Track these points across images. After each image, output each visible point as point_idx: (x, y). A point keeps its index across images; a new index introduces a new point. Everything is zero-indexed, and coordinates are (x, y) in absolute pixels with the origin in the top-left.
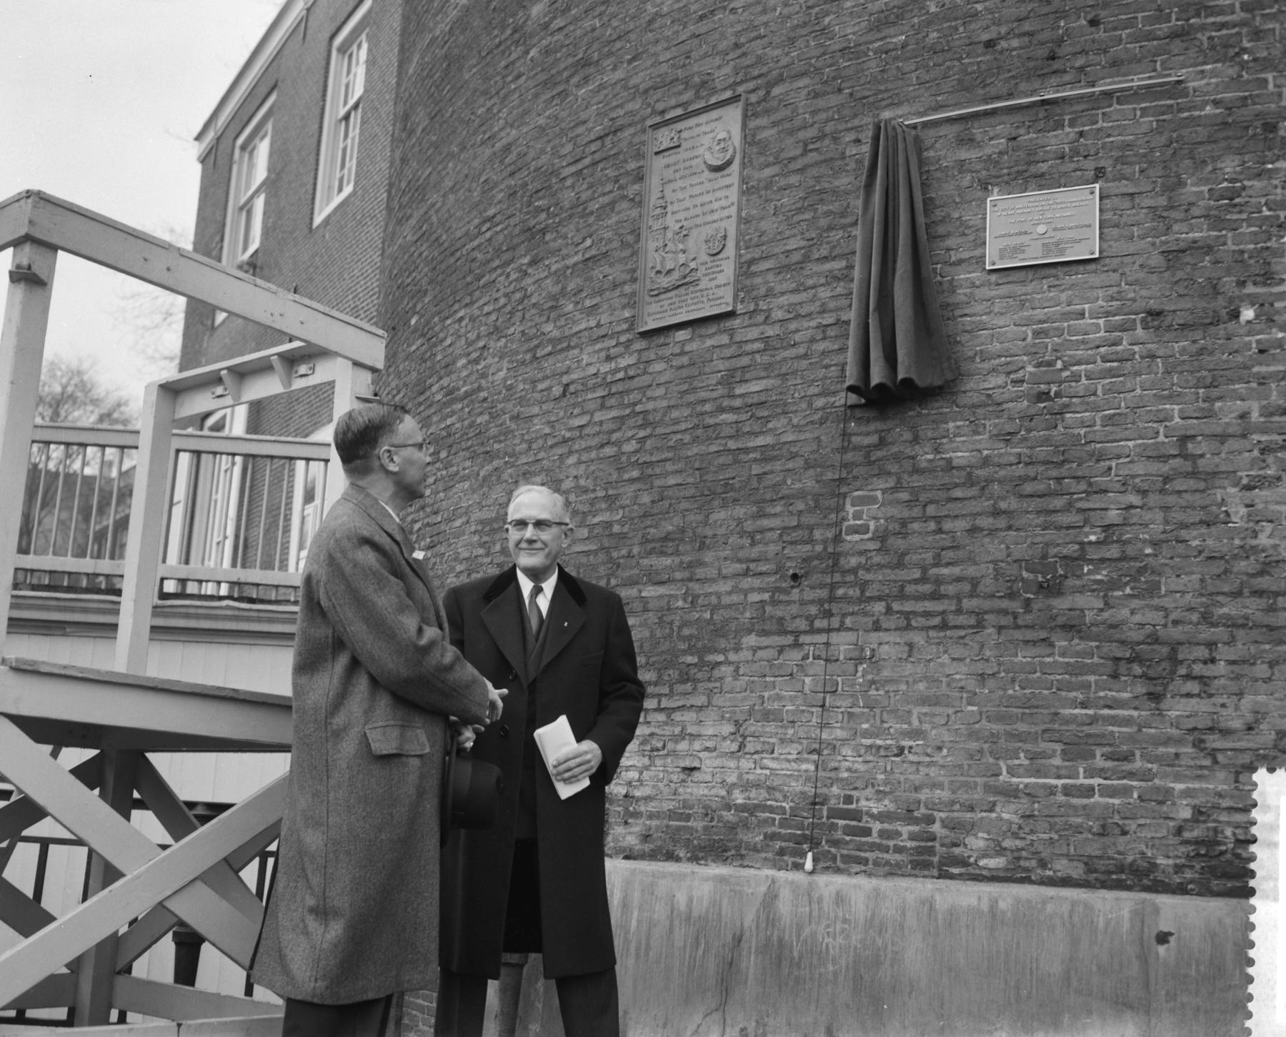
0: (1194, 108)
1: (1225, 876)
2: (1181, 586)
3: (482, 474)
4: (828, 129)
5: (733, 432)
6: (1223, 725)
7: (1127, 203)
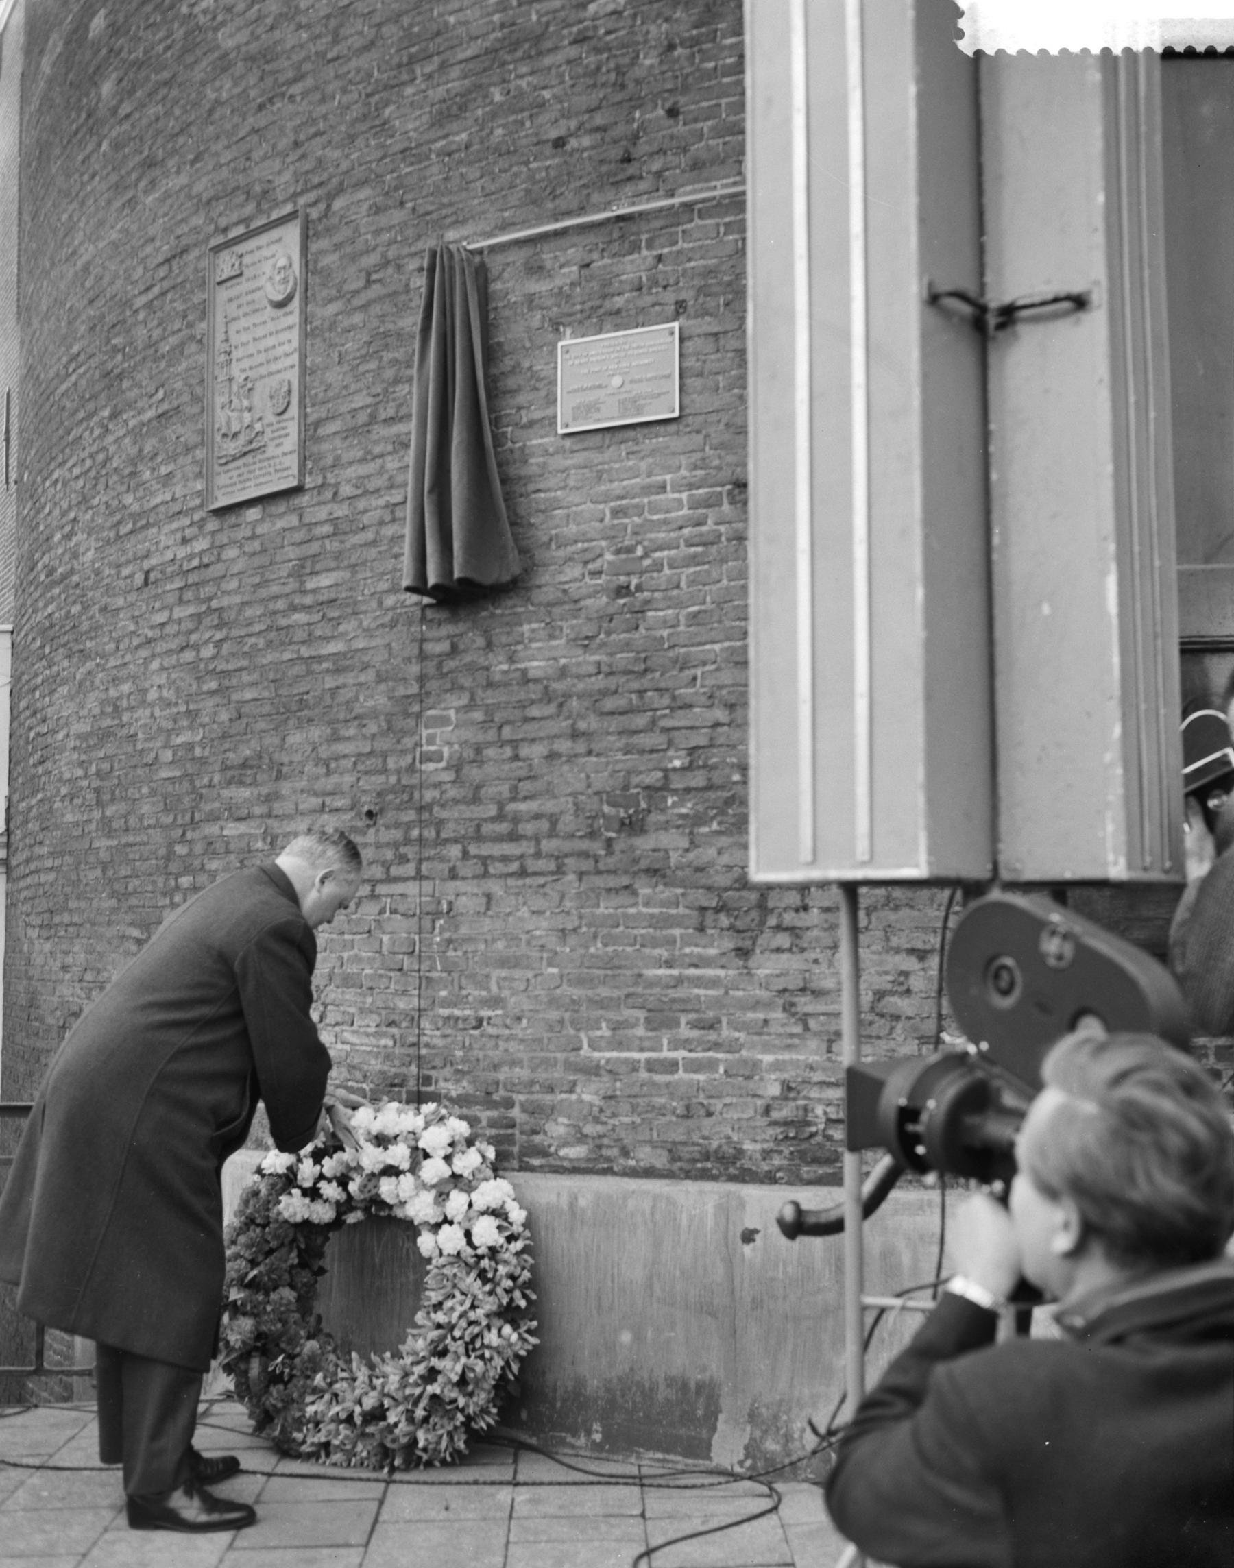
1: (816, 1161)
4: (391, 254)
5: (304, 636)
6: (814, 986)
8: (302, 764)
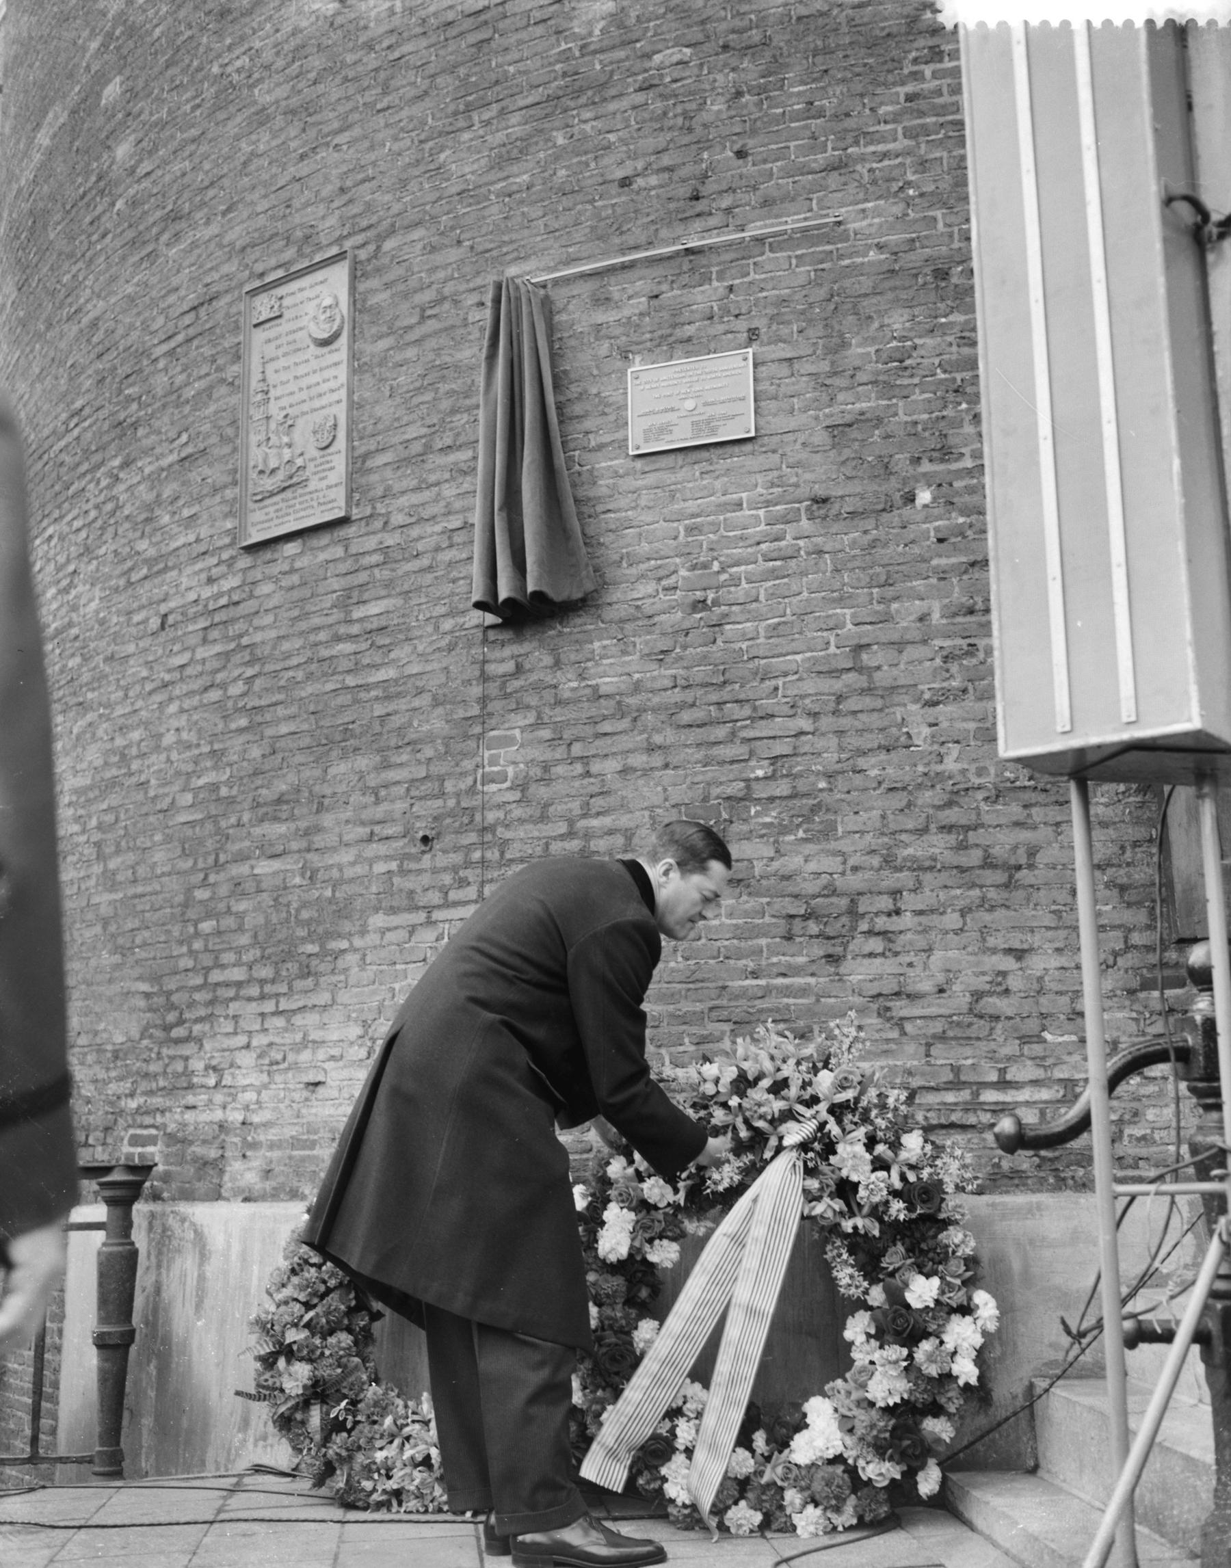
0: (856, 253)
2: (858, 829)
3: (75, 731)
5: (351, 665)
6: (909, 989)
7: (784, 370)
8: (347, 794)
